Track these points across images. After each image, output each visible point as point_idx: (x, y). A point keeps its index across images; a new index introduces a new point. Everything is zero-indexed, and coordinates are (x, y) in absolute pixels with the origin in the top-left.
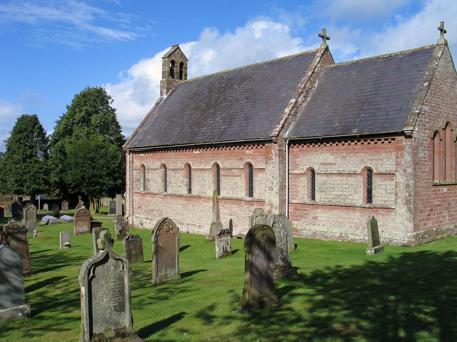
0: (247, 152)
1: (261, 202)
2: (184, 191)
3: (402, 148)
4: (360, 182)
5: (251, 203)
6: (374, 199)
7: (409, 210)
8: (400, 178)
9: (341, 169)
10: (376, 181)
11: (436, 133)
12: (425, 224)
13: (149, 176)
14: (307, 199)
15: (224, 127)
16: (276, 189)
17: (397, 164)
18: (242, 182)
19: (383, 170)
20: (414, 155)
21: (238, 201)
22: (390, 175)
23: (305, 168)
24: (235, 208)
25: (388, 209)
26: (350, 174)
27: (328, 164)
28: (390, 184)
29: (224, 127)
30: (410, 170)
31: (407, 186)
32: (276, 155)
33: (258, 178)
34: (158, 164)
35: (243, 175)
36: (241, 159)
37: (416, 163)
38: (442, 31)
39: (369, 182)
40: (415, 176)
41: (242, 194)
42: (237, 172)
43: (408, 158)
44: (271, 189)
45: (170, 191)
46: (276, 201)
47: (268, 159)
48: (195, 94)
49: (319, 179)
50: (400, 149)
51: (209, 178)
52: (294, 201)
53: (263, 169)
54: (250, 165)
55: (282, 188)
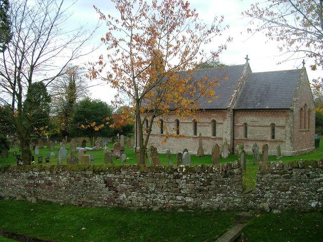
0: (213, 115)
4: (270, 129)
5: (215, 139)
6: (276, 137)
8: (287, 128)
10: (276, 129)
14: (243, 138)
16: (229, 132)
19: (280, 125)
21: (208, 138)
22: (283, 127)
23: (243, 123)
28: (283, 131)
32: (229, 117)
33: (218, 128)
35: (211, 126)
39: (273, 130)
42: (207, 124)
44: (226, 132)
47: (224, 118)
50: (288, 116)
51: (173, 126)
52: (236, 138)
54: (214, 121)
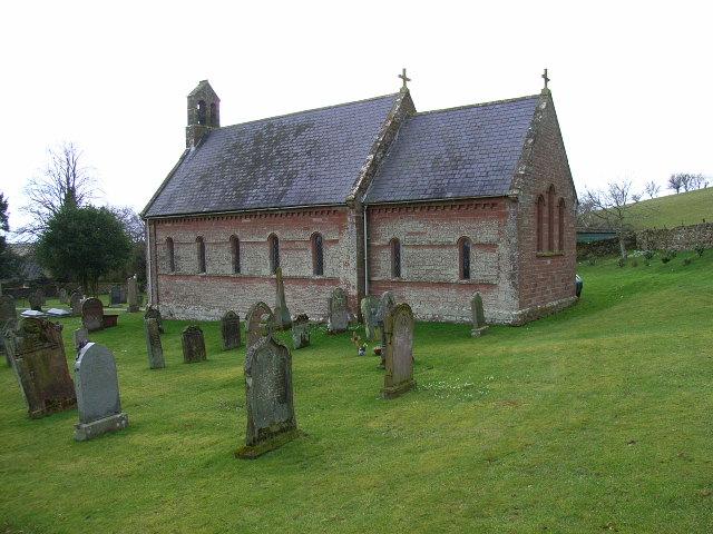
1: (334, 281)
2: (229, 270)
3: (505, 215)
5: (321, 282)
7: (514, 284)
8: (503, 249)
9: (432, 240)
10: (474, 252)
11: (541, 198)
12: (530, 301)
13: (179, 251)
15: (281, 189)
16: (353, 264)
17: (500, 233)
18: (308, 257)
20: (519, 223)
22: (491, 246)
23: (388, 239)
24: (299, 289)
25: (489, 286)
26: (443, 246)
27: (417, 234)
28: (491, 257)
29: (281, 189)
30: (514, 240)
31: (512, 258)
34: (193, 237)
36: (306, 229)
37: (520, 232)
38: (405, 79)
40: (519, 247)
41: (309, 272)
42: (303, 245)
43: (512, 226)
44: (347, 264)
45: (209, 270)
46: (353, 279)
47: (341, 228)
48: (235, 147)
49: (405, 252)
51: (264, 253)
53: (336, 242)
55: (361, 264)
